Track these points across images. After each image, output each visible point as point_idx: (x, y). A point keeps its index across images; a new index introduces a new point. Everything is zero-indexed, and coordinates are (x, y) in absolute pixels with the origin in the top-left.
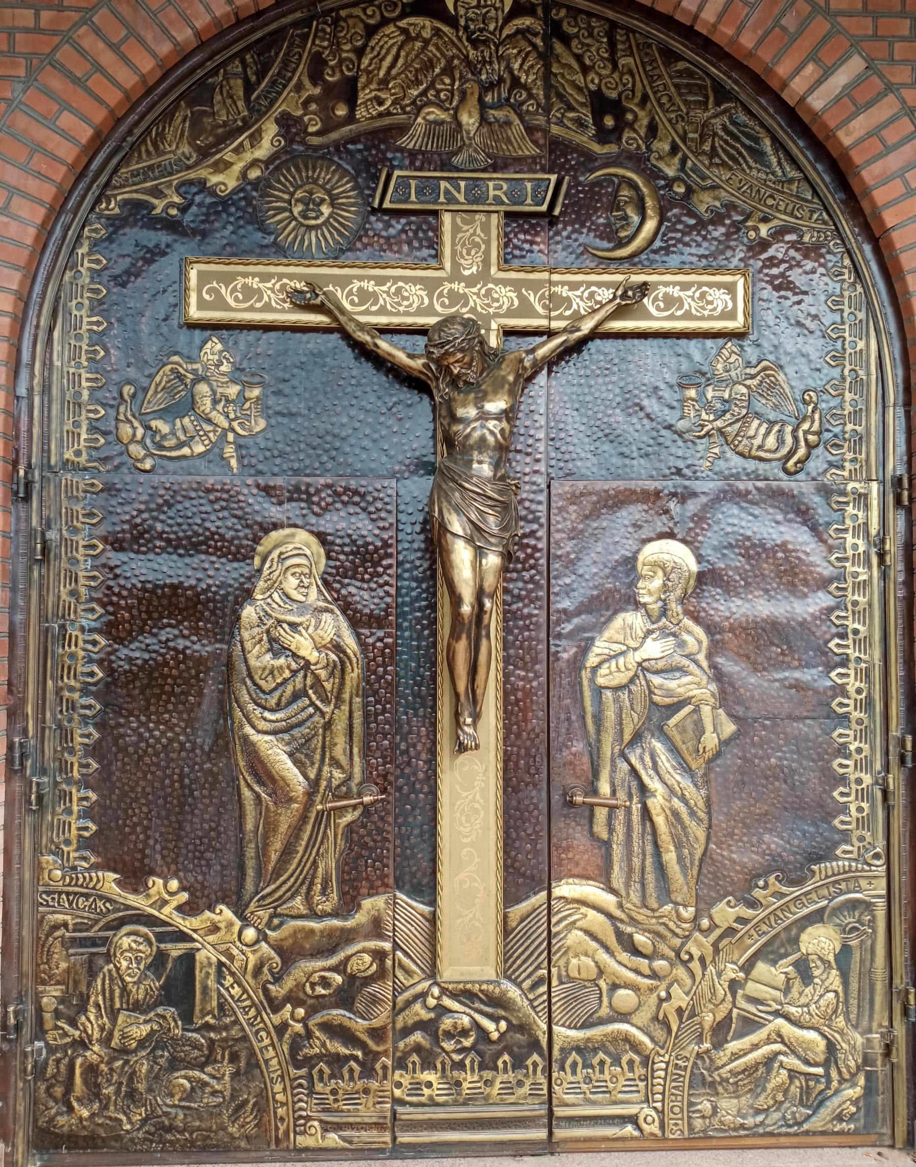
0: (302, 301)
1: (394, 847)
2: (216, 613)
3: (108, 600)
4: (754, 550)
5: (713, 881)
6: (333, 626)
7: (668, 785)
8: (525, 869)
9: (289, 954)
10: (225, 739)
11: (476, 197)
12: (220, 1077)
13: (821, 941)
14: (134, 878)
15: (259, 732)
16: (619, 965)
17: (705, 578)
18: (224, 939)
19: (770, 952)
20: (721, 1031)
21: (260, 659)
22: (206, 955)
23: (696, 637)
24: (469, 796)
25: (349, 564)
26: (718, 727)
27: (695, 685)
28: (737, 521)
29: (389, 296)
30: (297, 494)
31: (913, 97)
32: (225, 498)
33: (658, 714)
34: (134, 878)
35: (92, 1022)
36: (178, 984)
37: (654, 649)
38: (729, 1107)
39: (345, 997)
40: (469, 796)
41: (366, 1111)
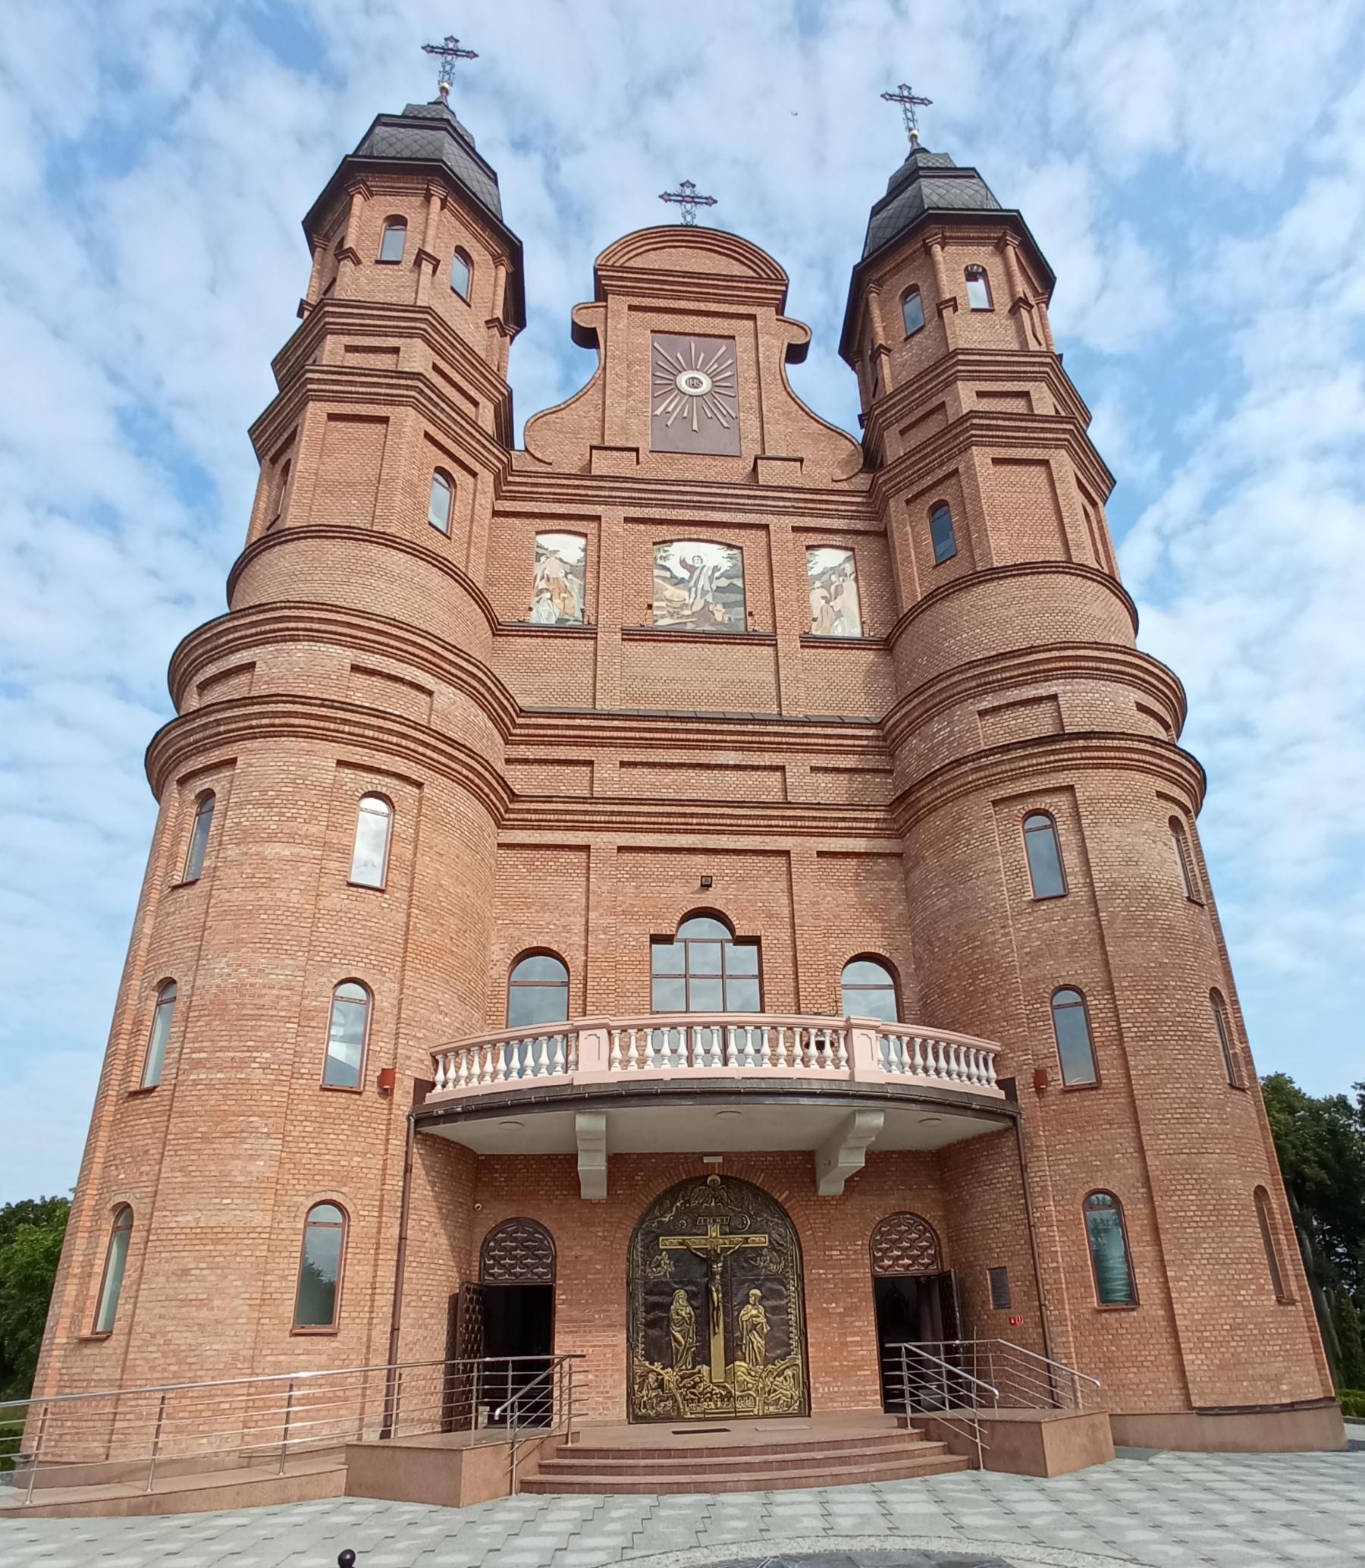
0: (680, 1244)
1: (703, 1356)
2: (666, 1307)
3: (645, 1305)
4: (771, 1290)
5: (767, 1361)
6: (689, 1309)
7: (758, 1341)
8: (729, 1359)
9: (683, 1378)
10: (669, 1333)
11: (715, 1221)
12: (670, 1403)
13: (789, 1372)
14: (652, 1364)
15: (511, 252)
16: (748, 1378)
17: (763, 1297)
18: (669, 1375)
19: (778, 1375)
20: (769, 1393)
21: (675, 1317)
22: (667, 1378)
23: (762, 1309)
24: (717, 1344)
25: (691, 1297)
26: (766, 1329)
27: (762, 1319)
28: (769, 1284)
29: (696, 1242)
30: (681, 1282)
31: (1364, 292)
32: (667, 1284)
33: (754, 1326)
34: (652, 1364)
35: (644, 1392)
36: (661, 1385)
37: (754, 1312)
38: (772, 1409)
39: (694, 1387)
40: (717, 1344)
41: (699, 1410)
